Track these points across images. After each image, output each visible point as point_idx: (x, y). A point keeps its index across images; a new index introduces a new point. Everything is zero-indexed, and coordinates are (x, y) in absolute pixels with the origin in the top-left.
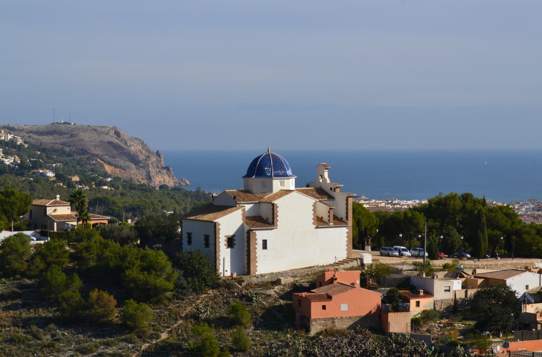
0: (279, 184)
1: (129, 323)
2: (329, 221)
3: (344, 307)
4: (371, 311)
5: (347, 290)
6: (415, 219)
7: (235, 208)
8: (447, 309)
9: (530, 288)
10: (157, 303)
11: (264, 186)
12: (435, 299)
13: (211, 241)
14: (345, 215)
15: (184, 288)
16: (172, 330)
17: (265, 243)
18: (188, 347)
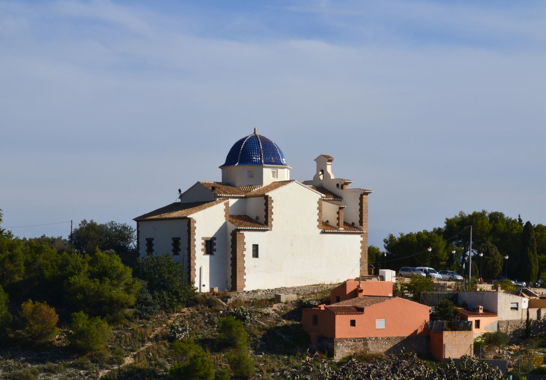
0: (271, 174)
1: (79, 342)
2: (338, 224)
3: (380, 324)
4: (417, 331)
5: (384, 300)
7: (214, 202)
8: (514, 333)
10: (113, 322)
12: (500, 319)
13: (183, 244)
14: (359, 219)
15: (149, 304)
16: (138, 353)
17: (256, 248)
18: (164, 373)
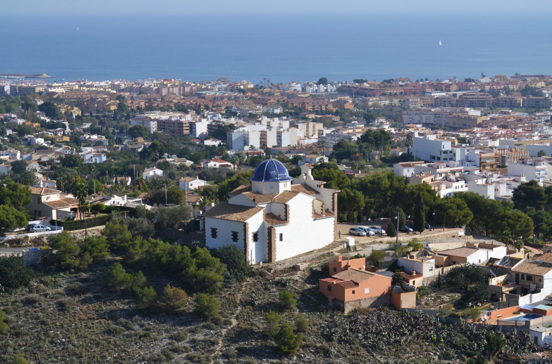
5: (368, 278)
6: (358, 197)
9: (481, 262)
11: (272, 188)
13: (240, 236)
17: (281, 235)
